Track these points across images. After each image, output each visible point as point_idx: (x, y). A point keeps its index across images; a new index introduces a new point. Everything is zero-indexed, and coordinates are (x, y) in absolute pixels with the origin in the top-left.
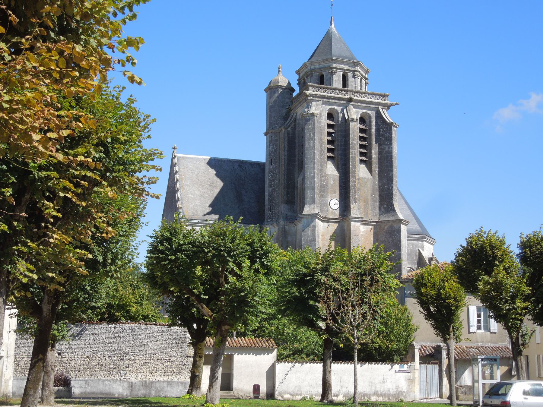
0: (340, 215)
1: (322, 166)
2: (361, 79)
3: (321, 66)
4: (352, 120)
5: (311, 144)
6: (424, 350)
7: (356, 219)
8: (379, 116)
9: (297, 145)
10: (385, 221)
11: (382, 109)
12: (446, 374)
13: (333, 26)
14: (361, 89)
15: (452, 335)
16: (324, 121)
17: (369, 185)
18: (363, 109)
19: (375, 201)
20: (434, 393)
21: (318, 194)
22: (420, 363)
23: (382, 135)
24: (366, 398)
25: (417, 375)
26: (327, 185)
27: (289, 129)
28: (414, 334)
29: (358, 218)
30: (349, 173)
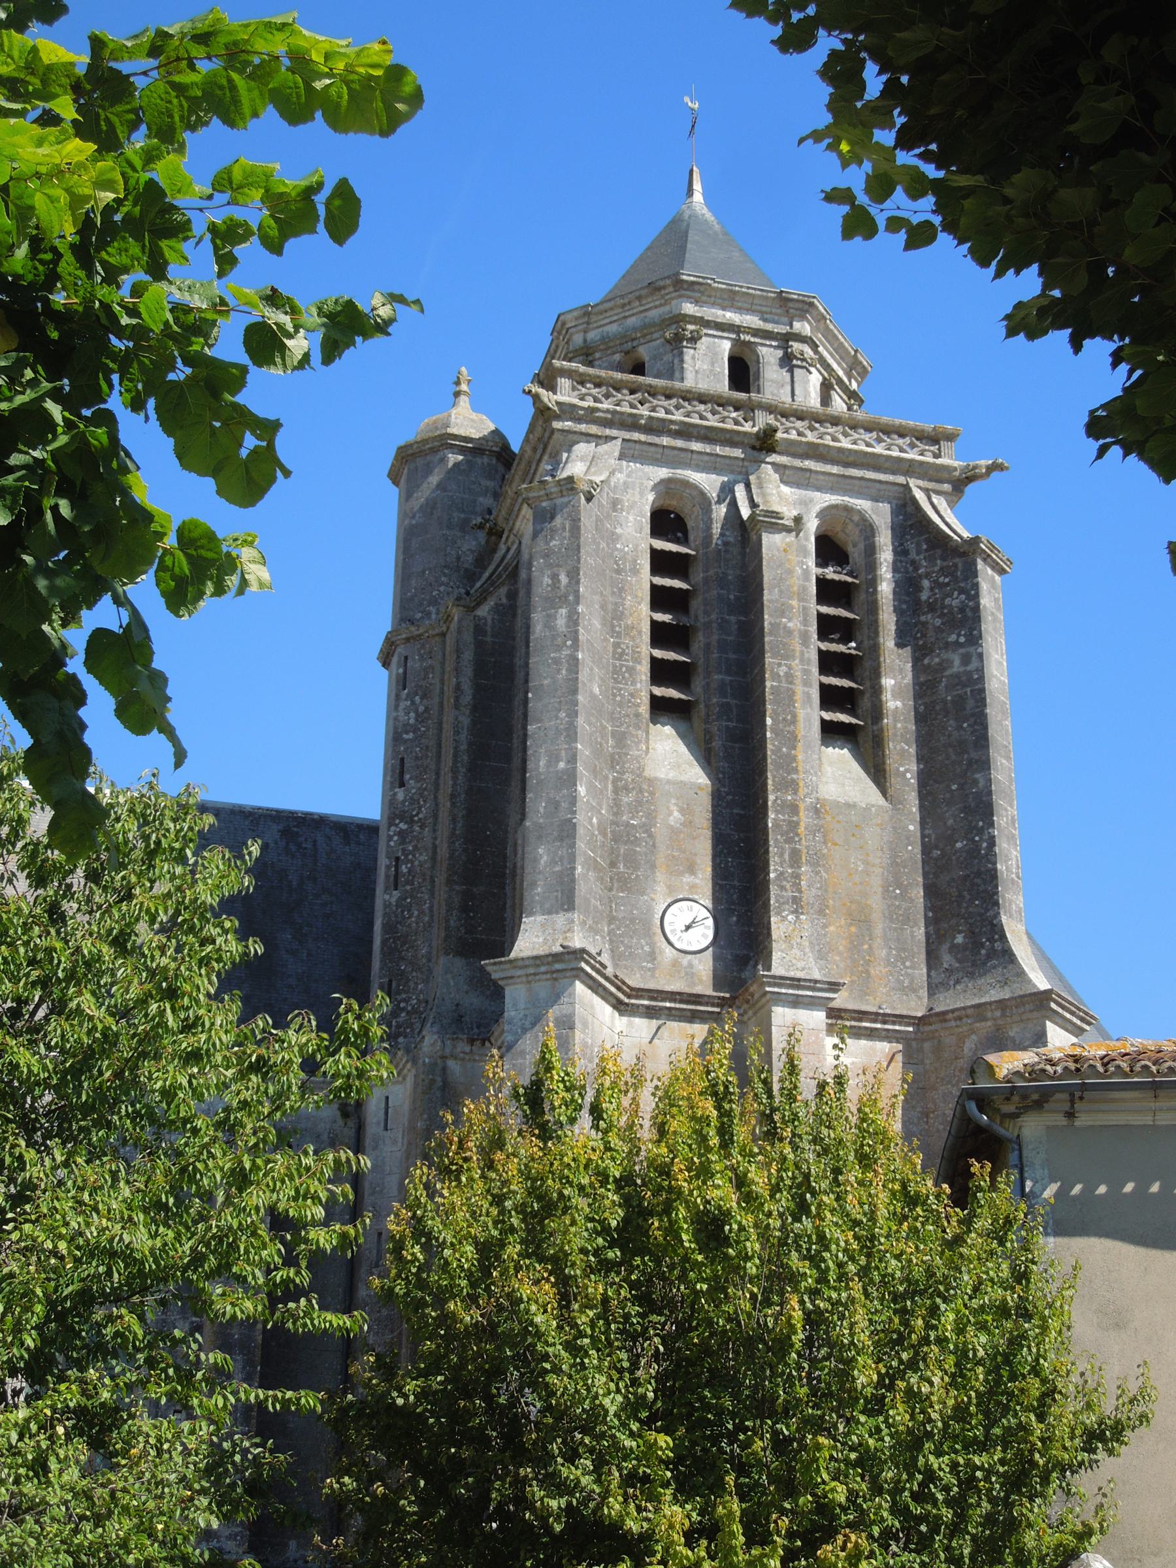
0: (719, 982)
1: (621, 739)
3: (632, 321)
4: (773, 521)
5: (561, 622)
7: (801, 992)
8: (911, 524)
10: (959, 1014)
11: (927, 491)
13: (698, 197)
16: (634, 536)
17: (874, 837)
18: (832, 490)
19: (907, 919)
21: (593, 865)
23: (932, 608)
26: (647, 828)
27: (483, 611)
29: (813, 984)
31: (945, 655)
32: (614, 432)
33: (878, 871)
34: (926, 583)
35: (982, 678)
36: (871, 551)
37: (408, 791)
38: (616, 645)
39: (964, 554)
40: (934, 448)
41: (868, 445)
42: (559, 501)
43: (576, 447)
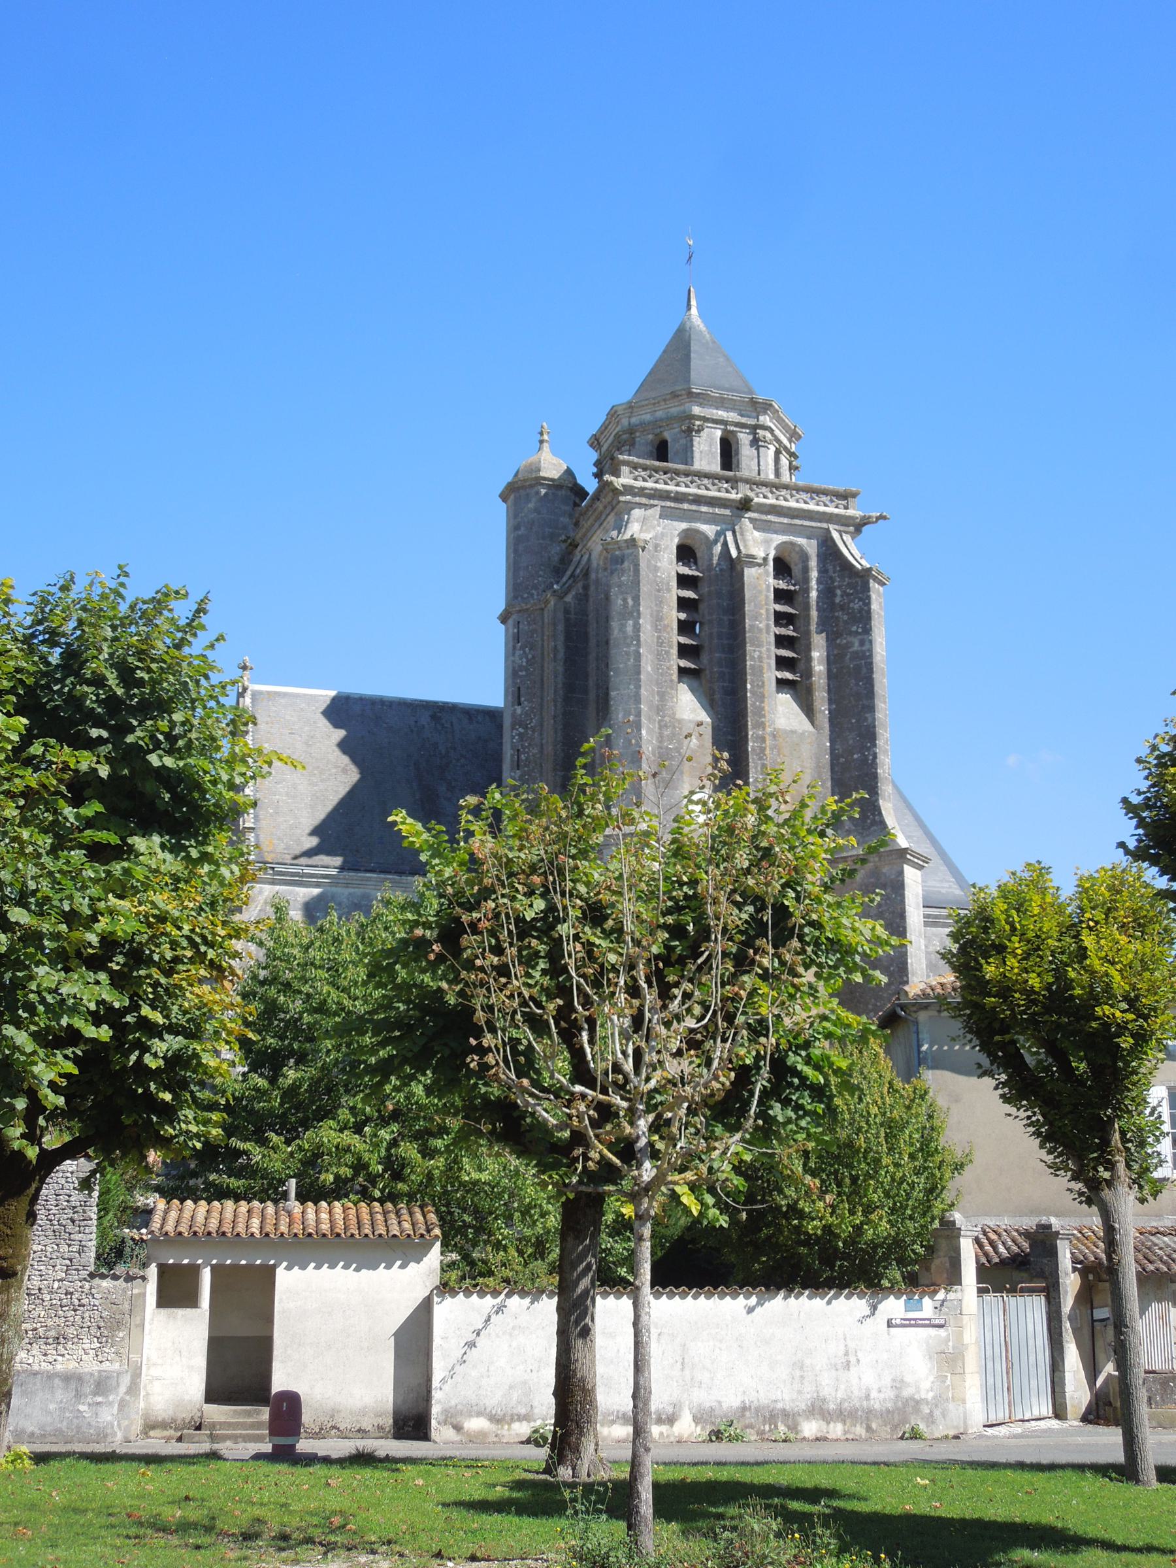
1: (662, 696)
2: (778, 453)
3: (659, 414)
4: (751, 560)
5: (629, 629)
6: (992, 1243)
8: (830, 553)
9: (592, 642)
11: (840, 532)
12: (1076, 1331)
13: (694, 311)
14: (777, 473)
15: (1121, 1166)
16: (668, 566)
18: (784, 532)
20: (1034, 1400)
22: (981, 1291)
24: (782, 1428)
25: (971, 1334)
27: (568, 598)
28: (954, 1185)
30: (745, 716)
31: (850, 639)
32: (656, 502)
33: (809, 771)
34: (839, 592)
35: (871, 656)
36: (806, 570)
37: (523, 708)
38: (659, 638)
39: (862, 577)
40: (844, 502)
41: (806, 502)
42: (627, 552)
43: (633, 512)
